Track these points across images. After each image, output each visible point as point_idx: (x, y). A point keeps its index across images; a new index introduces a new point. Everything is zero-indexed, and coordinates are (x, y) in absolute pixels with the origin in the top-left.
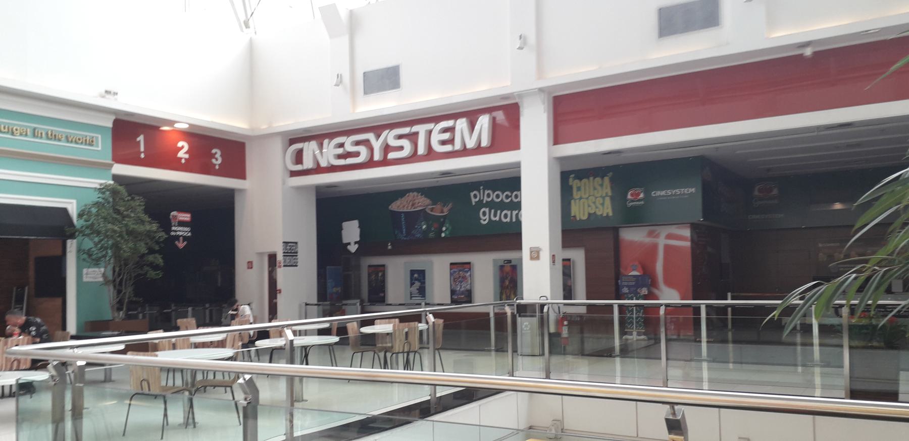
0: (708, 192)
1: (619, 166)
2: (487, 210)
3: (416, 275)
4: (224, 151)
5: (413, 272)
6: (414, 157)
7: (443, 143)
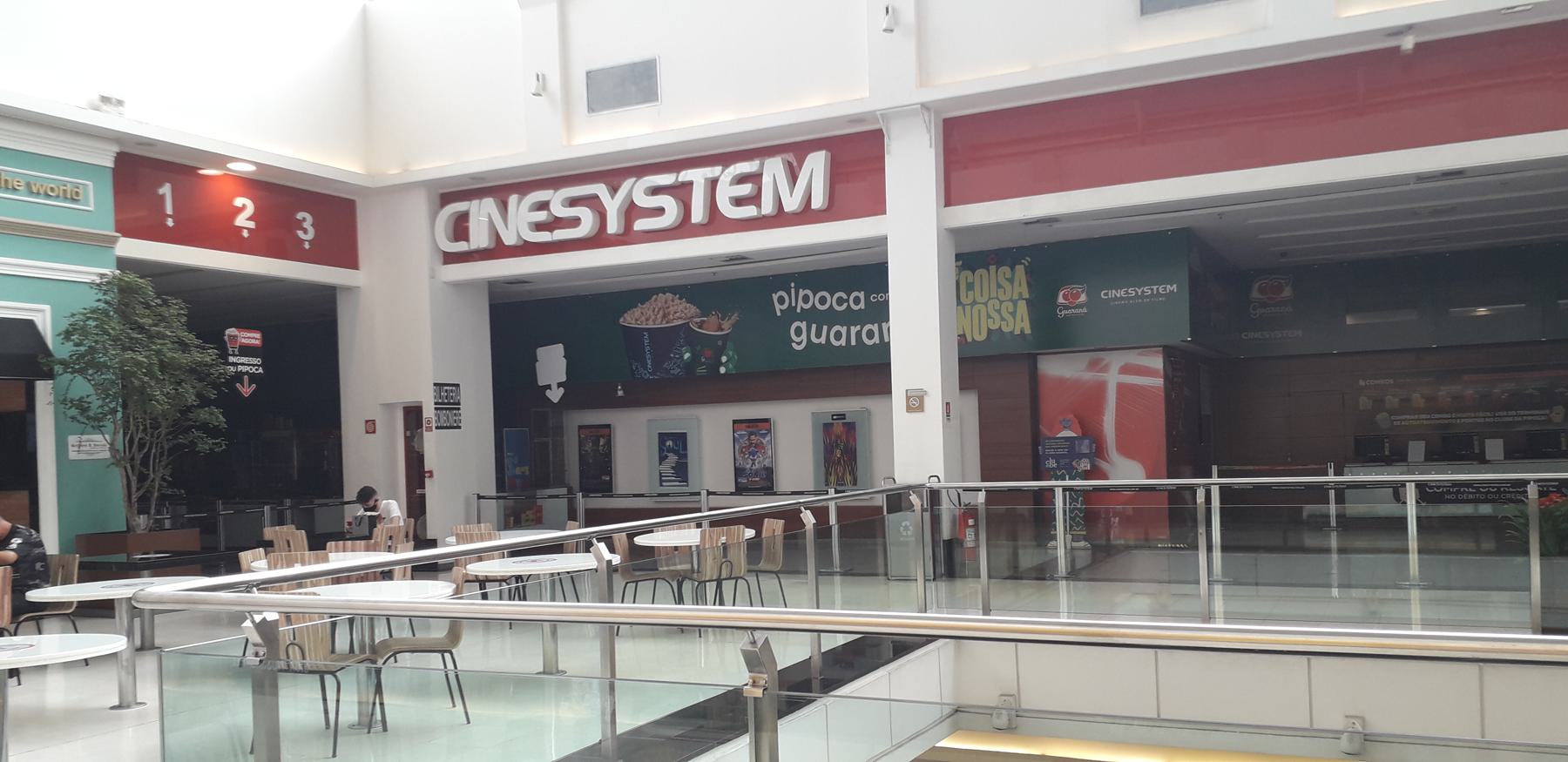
0: (1196, 286)
2: (803, 325)
5: (663, 437)
6: (683, 229)
7: (738, 202)
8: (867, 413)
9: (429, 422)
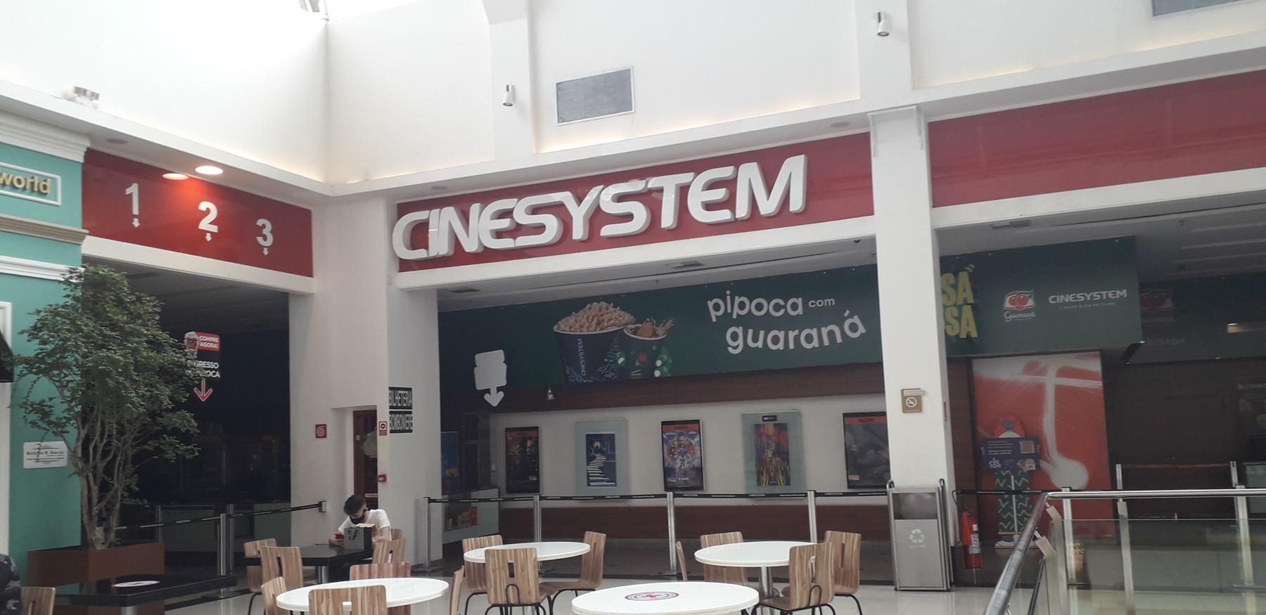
1: (986, 253)
2: (740, 331)
3: (597, 444)
4: (271, 219)
5: (590, 439)
6: (652, 233)
7: (709, 206)
8: (797, 415)
9: (383, 426)
